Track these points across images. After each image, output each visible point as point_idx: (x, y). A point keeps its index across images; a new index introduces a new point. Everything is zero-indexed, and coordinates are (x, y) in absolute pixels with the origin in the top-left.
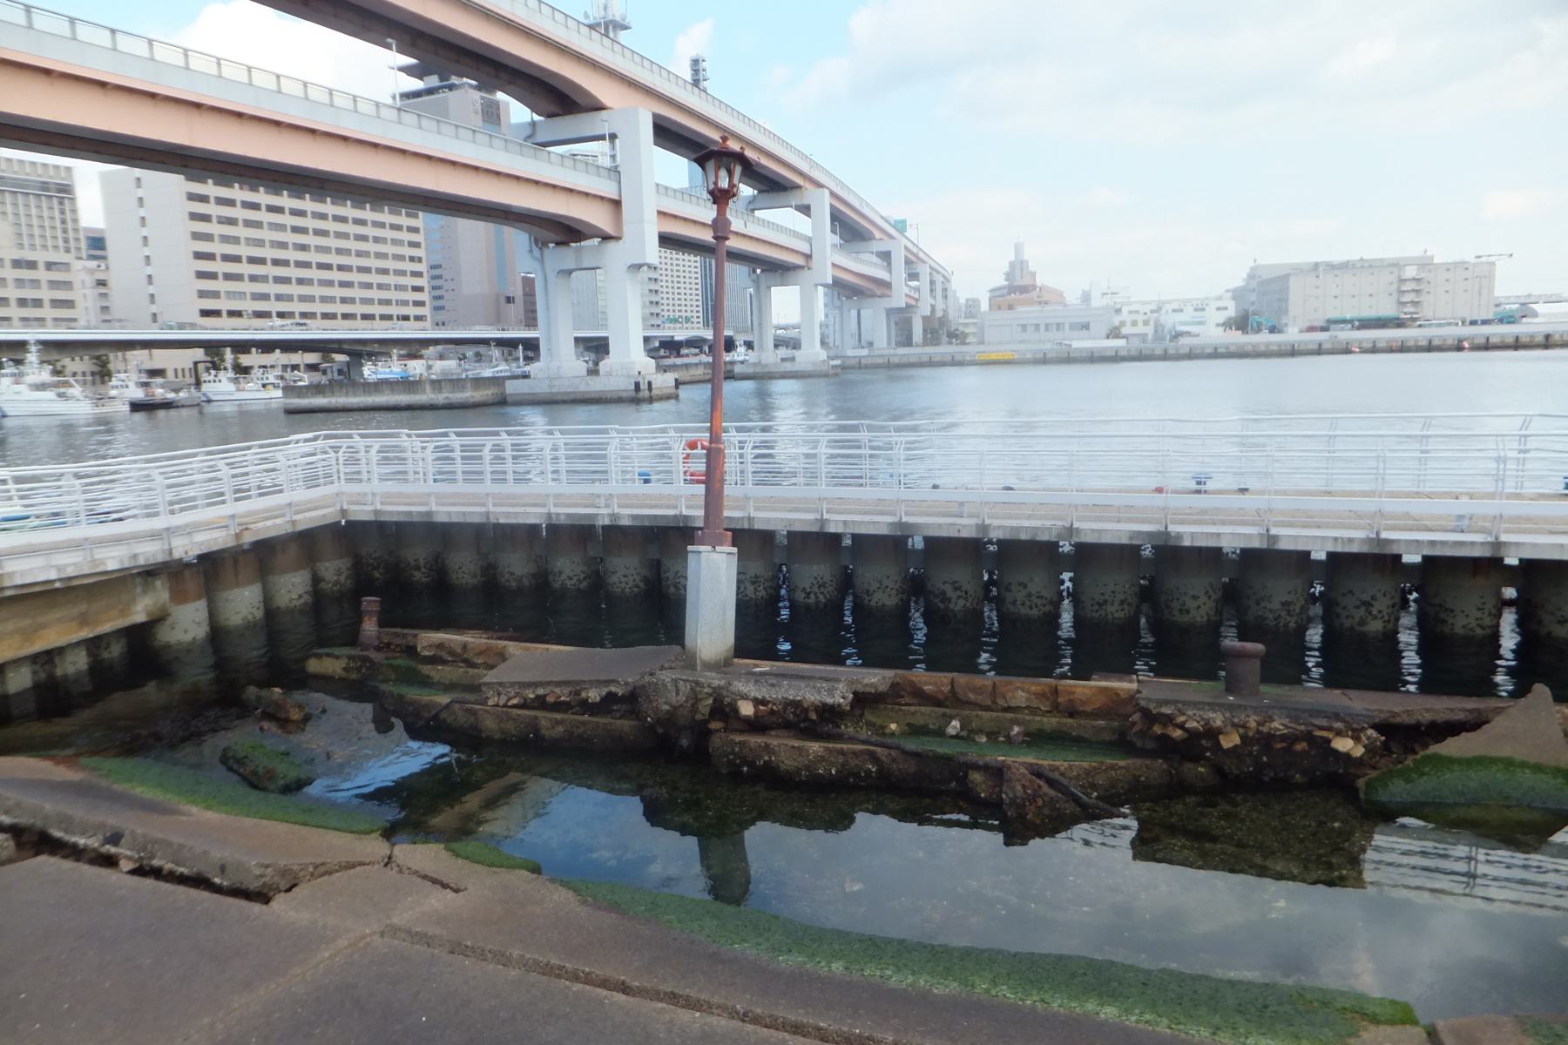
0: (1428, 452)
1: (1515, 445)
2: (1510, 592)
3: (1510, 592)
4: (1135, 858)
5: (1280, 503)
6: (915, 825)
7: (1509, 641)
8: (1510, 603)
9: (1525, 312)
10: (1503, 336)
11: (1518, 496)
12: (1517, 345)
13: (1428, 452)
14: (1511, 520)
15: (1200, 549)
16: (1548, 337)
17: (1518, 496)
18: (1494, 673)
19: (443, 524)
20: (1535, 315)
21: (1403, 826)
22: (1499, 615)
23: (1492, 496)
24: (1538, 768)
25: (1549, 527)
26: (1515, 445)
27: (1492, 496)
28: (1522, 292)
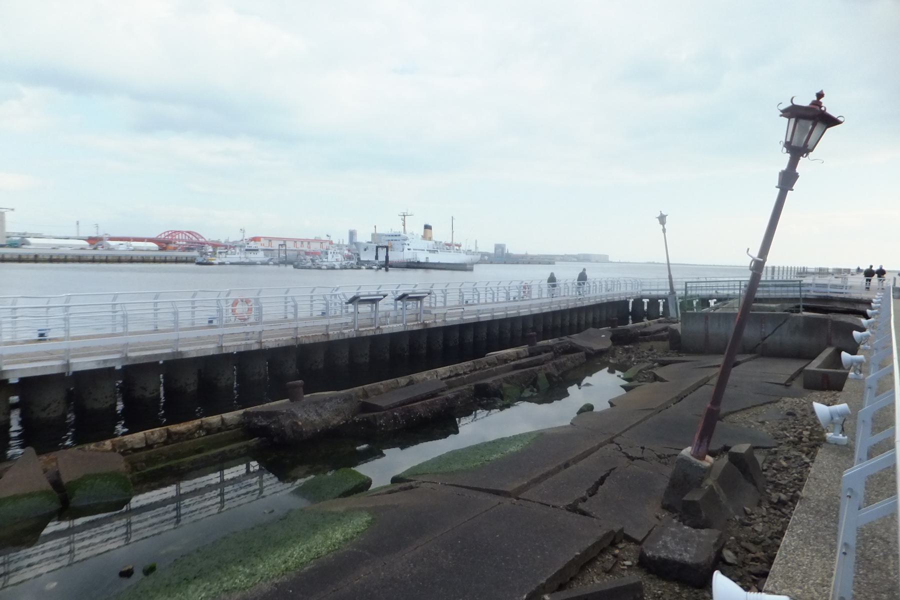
0: (16, 317)
1: (190, 305)
2: (14, 399)
3: (14, 399)
4: (457, 432)
5: (133, 339)
6: (398, 449)
7: (15, 425)
8: (14, 406)
9: (22, 242)
10: (12, 254)
11: (13, 343)
12: (20, 260)
13: (16, 317)
14: (11, 356)
15: (201, 357)
16: (36, 256)
17: (13, 343)
18: (8, 447)
19: (335, 341)
20: (29, 244)
21: (46, 536)
22: (9, 414)
23: (62, 339)
24: (31, 495)
25: (30, 358)
26: (152, 307)
27: (173, 330)
28: (21, 230)
